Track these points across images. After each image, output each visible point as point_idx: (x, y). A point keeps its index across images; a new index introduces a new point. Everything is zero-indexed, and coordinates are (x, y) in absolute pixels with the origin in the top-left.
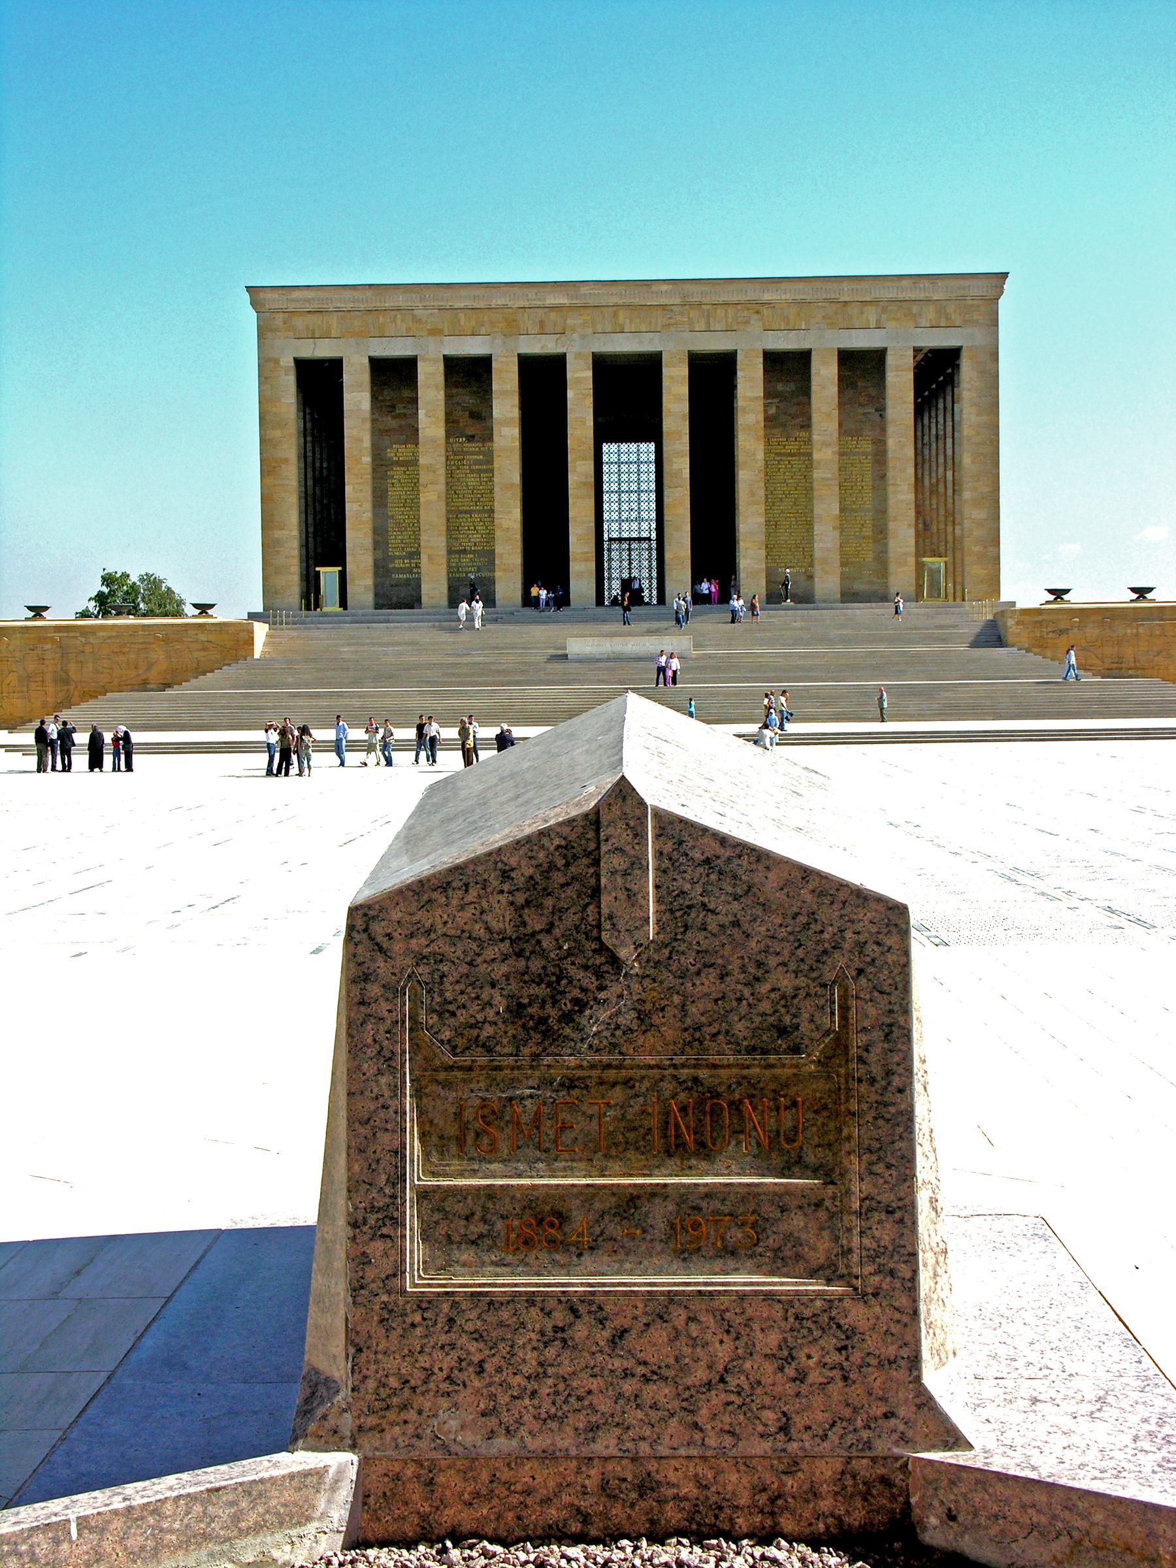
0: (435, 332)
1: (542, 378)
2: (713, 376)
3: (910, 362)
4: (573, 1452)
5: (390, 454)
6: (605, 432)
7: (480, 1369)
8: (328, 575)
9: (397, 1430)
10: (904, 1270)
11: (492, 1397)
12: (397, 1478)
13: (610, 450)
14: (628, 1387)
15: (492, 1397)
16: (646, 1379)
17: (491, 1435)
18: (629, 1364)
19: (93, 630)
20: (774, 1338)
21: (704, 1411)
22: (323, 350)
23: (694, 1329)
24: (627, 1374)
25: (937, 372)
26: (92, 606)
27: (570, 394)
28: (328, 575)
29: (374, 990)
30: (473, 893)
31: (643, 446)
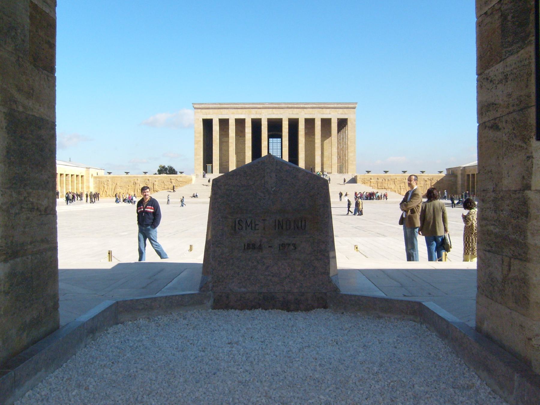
0: (233, 113)
1: (256, 124)
2: (294, 124)
3: (336, 121)
4: (258, 291)
5: (223, 140)
6: (270, 136)
7: (238, 274)
8: (209, 166)
9: (221, 286)
10: (327, 254)
11: (241, 280)
12: (221, 296)
13: (271, 140)
14: (269, 278)
15: (241, 280)
16: (273, 276)
17: (240, 288)
18: (270, 273)
19: (157, 177)
20: (299, 269)
21: (285, 283)
22: (208, 117)
23: (283, 266)
24: (269, 275)
25: (342, 123)
26: (157, 173)
27: (262, 127)
28: (209, 166)
29: (218, 196)
30: (238, 177)
31: (278, 139)
